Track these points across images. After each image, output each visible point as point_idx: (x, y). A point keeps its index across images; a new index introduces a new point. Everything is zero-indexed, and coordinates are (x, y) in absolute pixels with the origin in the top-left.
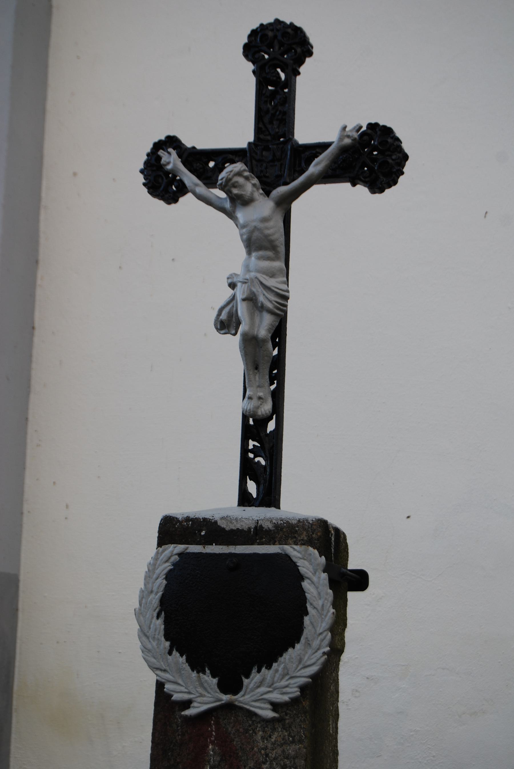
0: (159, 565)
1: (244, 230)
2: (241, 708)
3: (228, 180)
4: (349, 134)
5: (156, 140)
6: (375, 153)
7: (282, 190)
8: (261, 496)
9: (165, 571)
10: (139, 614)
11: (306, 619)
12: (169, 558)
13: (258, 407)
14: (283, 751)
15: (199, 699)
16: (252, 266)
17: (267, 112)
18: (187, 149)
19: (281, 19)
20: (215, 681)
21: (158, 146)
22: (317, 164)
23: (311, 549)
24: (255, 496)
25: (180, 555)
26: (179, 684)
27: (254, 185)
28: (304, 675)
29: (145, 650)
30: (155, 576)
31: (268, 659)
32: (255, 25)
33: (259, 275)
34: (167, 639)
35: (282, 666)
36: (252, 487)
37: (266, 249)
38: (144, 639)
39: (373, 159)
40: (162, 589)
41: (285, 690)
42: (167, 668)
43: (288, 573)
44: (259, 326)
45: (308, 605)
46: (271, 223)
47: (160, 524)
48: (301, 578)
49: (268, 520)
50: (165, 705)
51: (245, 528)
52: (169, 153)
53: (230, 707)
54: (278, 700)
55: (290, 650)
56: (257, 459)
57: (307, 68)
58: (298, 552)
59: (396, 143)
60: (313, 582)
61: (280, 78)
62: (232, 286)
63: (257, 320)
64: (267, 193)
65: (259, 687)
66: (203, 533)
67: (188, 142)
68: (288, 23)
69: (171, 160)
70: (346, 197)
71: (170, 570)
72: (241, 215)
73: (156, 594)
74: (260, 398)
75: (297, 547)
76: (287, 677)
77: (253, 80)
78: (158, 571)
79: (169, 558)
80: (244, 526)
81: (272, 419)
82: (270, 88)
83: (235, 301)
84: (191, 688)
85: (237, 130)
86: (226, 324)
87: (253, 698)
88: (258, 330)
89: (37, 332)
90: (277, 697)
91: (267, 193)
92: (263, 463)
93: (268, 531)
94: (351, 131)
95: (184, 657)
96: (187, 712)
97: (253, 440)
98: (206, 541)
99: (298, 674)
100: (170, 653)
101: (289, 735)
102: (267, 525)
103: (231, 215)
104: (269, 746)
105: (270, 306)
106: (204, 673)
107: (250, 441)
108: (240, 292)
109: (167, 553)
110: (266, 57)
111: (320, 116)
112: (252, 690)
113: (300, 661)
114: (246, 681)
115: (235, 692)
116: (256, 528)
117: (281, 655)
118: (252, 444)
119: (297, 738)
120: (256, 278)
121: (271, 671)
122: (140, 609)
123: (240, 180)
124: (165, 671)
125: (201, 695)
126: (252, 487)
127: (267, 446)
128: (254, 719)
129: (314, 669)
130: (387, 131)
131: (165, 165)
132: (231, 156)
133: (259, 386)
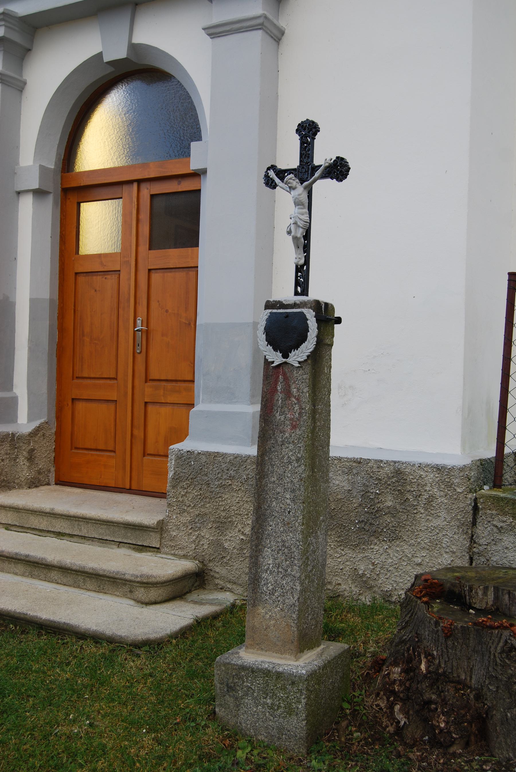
3: (287, 181)
7: (306, 183)
16: (296, 212)
17: (304, 154)
21: (268, 169)
28: (308, 352)
31: (297, 347)
33: (298, 215)
36: (299, 289)
37: (300, 205)
39: (338, 170)
43: (303, 318)
48: (307, 320)
53: (285, 363)
59: (346, 163)
63: (298, 230)
64: (302, 184)
69: (272, 174)
70: (330, 183)
72: (293, 192)
84: (274, 357)
91: (302, 184)
93: (298, 304)
96: (272, 365)
102: (298, 302)
103: (290, 193)
105: (301, 226)
109: (266, 313)
114: (290, 354)
115: (287, 358)
118: (299, 274)
123: (291, 181)
126: (299, 289)
127: (303, 275)
129: (311, 350)
130: (342, 159)
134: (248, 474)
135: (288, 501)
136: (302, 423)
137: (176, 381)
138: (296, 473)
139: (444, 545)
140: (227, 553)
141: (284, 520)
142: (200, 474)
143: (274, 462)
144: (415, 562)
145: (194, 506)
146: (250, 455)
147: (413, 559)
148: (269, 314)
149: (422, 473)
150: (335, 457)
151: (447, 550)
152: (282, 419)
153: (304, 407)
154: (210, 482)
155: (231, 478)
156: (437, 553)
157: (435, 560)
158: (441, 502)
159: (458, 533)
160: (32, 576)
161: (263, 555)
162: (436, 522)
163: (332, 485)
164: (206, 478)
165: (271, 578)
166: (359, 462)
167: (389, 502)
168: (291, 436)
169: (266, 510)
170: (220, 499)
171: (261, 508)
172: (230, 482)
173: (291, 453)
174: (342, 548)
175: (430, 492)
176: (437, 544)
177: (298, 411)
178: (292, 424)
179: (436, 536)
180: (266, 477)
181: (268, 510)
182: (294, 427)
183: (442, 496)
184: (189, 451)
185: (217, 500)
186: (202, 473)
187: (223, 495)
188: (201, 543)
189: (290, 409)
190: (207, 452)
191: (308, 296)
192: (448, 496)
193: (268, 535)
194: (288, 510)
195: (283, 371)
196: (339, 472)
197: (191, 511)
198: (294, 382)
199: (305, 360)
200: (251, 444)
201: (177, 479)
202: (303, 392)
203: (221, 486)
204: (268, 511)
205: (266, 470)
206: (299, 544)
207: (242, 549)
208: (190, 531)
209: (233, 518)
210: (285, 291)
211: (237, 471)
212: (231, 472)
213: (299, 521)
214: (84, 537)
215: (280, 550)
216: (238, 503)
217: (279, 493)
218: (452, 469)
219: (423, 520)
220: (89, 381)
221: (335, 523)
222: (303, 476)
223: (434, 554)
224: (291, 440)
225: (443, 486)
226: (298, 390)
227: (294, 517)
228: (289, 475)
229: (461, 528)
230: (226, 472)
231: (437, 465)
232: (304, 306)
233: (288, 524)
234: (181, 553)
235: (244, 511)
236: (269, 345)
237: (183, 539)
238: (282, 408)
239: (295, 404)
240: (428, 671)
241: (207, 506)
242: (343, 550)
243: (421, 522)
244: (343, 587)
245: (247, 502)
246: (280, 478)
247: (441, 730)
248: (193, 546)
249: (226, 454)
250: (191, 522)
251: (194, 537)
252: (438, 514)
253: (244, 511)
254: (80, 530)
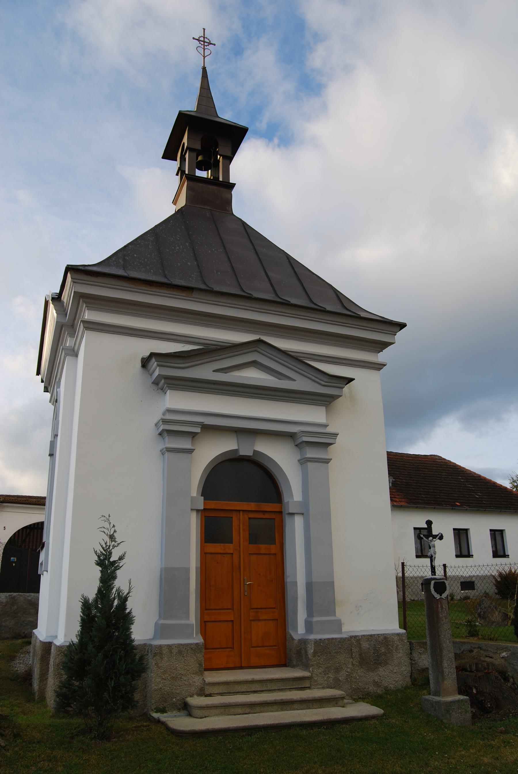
31: (444, 592)
137: (266, 608)
160: (282, 710)
162: (399, 655)
165: (447, 670)
166: (371, 636)
167: (383, 650)
182: (446, 618)
201: (315, 653)
203: (335, 652)
207: (347, 679)
214: (270, 690)
218: (402, 634)
220: (214, 611)
234: (321, 687)
240: (477, 692)
244: (371, 688)
247: (489, 707)
254: (267, 687)
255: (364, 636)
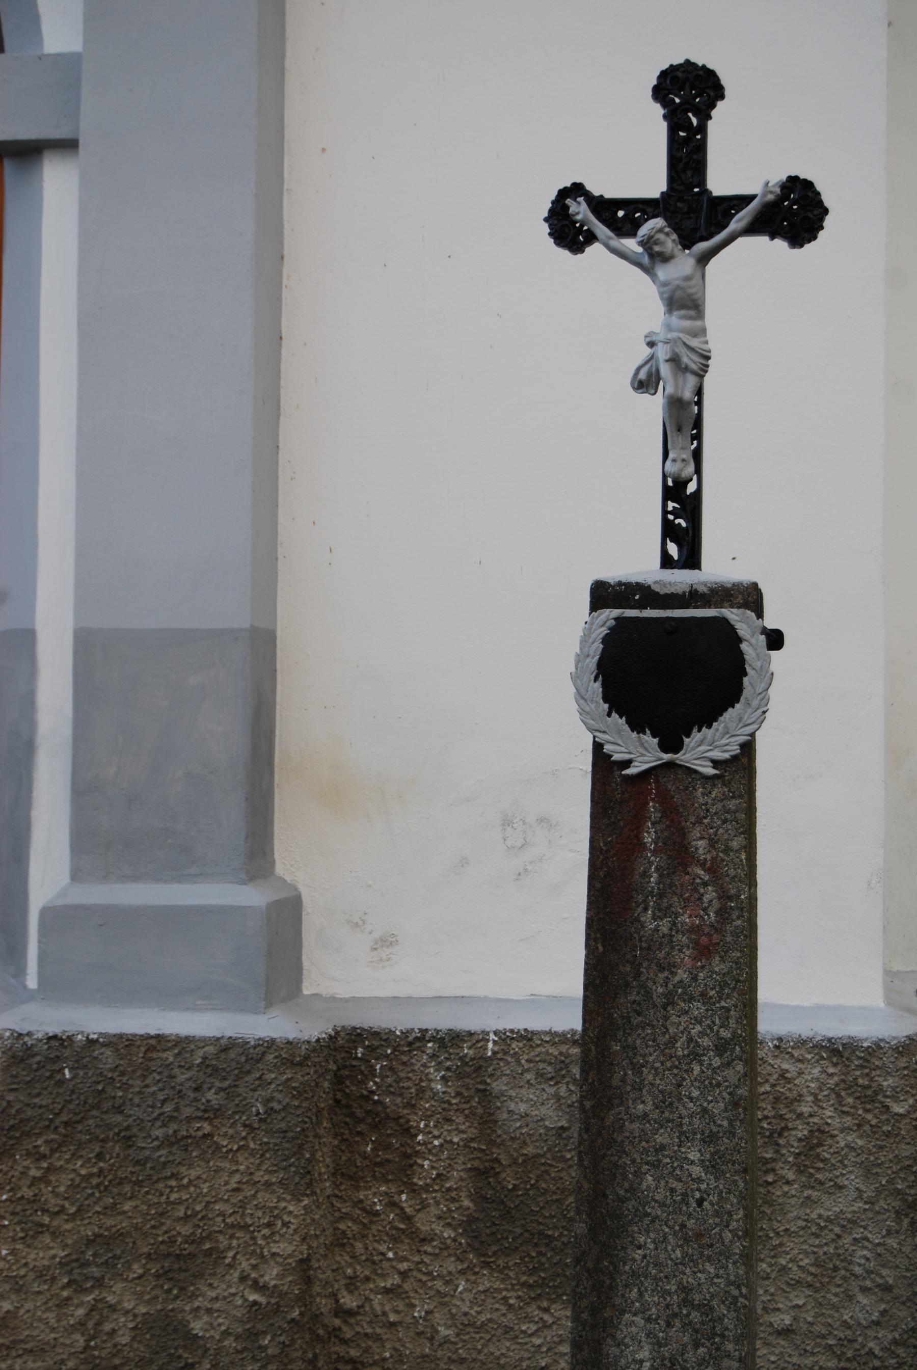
0: (595, 630)
1: (666, 289)
2: (681, 766)
4: (772, 189)
5: (561, 187)
6: (795, 207)
7: (702, 246)
8: (684, 557)
9: (602, 636)
10: (575, 678)
11: (746, 680)
12: (605, 622)
13: (682, 470)
14: (724, 806)
15: (640, 759)
18: (594, 197)
19: (692, 60)
20: (656, 740)
21: (564, 194)
22: (739, 220)
23: (748, 612)
24: (676, 557)
25: (616, 619)
26: (619, 745)
27: (674, 241)
29: (582, 712)
30: (591, 640)
31: (708, 718)
32: (665, 66)
33: (681, 335)
34: (605, 702)
35: (723, 725)
38: (582, 702)
39: (795, 213)
40: (599, 652)
41: (725, 748)
42: (606, 730)
43: (729, 637)
44: (683, 388)
45: (747, 666)
46: (693, 282)
47: (591, 589)
48: (740, 640)
49: (702, 584)
50: (604, 765)
51: (680, 591)
52: (579, 203)
53: (670, 765)
54: (719, 758)
55: (730, 710)
56: (677, 521)
57: (720, 111)
58: (736, 615)
60: (751, 645)
61: (692, 124)
62: (651, 344)
63: (681, 381)
65: (699, 745)
66: (637, 597)
67: (596, 189)
68: (700, 65)
69: (579, 209)
71: (607, 634)
73: (593, 658)
74: (683, 460)
75: (735, 610)
76: (728, 736)
77: (663, 126)
78: (594, 636)
79: (605, 622)
80: (679, 590)
81: (691, 480)
82: (682, 134)
83: (653, 361)
84: (631, 748)
85: (652, 182)
86: (646, 383)
87: (695, 756)
88: (682, 392)
89: (284, 342)
90: (718, 755)
92: (684, 524)
93: (703, 595)
94: (774, 186)
95: (624, 718)
97: (673, 502)
98: (642, 606)
99: (738, 733)
100: (609, 715)
101: (729, 791)
102: (702, 589)
104: (710, 801)
105: (694, 366)
106: (644, 733)
107: (669, 502)
108: (662, 352)
110: (677, 100)
111: (737, 166)
112: (693, 749)
113: (740, 720)
116: (690, 592)
117: (721, 715)
119: (737, 793)
120: (679, 338)
121: (712, 730)
122: (576, 673)
123: (661, 236)
124: (604, 732)
125: (642, 755)
128: (693, 776)
130: (808, 185)
131: (574, 215)
132: (641, 206)
133: (682, 448)
134: (272, 1099)
135: (697, 1171)
136: (729, 939)
138: (719, 1085)
139: (858, 1270)
140: (200, 1352)
141: (683, 1226)
142: (97, 1107)
143: (644, 1056)
144: (771, 1324)
145: (79, 1210)
146: (273, 1041)
147: (766, 1318)
148: (612, 623)
149: (785, 1066)
150: (512, 1031)
151: (868, 1283)
152: (665, 930)
153: (733, 892)
154: (135, 1130)
155: (212, 1113)
156: (836, 1295)
157: (830, 1316)
158: (847, 1146)
159: (897, 1232)
161: (620, 1336)
162: (833, 1206)
163: (505, 1116)
164: (119, 1118)
168: (695, 978)
169: (622, 1200)
170: (173, 1183)
171: (605, 1196)
172: (207, 1128)
173: (698, 1028)
174: (545, 1304)
175: (811, 1120)
176: (836, 1269)
177: (716, 905)
178: (697, 943)
179: (833, 1246)
180: (617, 1102)
181: (629, 1199)
183: (849, 1128)
184: (55, 1037)
185: (161, 1185)
186: (106, 1105)
187: (183, 1169)
188: (107, 1327)
189: (688, 900)
190: (121, 1036)
191: (700, 568)
192: (867, 1128)
193: (634, 1274)
194: (697, 1195)
195: (657, 788)
196: (528, 1076)
197: (68, 1226)
198: (699, 821)
199: (733, 757)
200: (263, 1004)
202: (727, 850)
204: (630, 1205)
205: (615, 1082)
206: (736, 1293)
207: (253, 1335)
208: (65, 1294)
209: (221, 1238)
210: (637, 556)
211: (229, 1092)
212: (210, 1095)
213: (734, 1225)
215: (675, 1315)
216: (237, 1190)
217: (663, 1147)
218: (877, 1048)
219: (793, 1201)
221: (518, 1231)
222: (739, 1092)
223: (829, 1296)
224: (696, 991)
225: (850, 1100)
226: (712, 843)
227: (717, 1214)
228: (696, 1093)
229: (907, 1215)
230: (192, 1095)
231: (830, 1040)
232: (722, 601)
233: (699, 1235)
235: (260, 1214)
236: (615, 715)
237: (40, 1320)
238: (661, 896)
239: (705, 884)
241: (126, 1208)
242: (546, 1310)
243: (788, 1208)
245: (268, 1184)
246: (665, 1102)
248: (80, 1340)
249: (189, 1040)
250: (67, 1264)
251: (81, 1312)
252: (839, 1181)
253: (260, 1214)
255: (527, 1037)
